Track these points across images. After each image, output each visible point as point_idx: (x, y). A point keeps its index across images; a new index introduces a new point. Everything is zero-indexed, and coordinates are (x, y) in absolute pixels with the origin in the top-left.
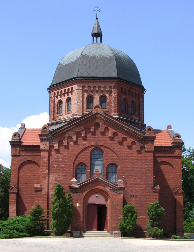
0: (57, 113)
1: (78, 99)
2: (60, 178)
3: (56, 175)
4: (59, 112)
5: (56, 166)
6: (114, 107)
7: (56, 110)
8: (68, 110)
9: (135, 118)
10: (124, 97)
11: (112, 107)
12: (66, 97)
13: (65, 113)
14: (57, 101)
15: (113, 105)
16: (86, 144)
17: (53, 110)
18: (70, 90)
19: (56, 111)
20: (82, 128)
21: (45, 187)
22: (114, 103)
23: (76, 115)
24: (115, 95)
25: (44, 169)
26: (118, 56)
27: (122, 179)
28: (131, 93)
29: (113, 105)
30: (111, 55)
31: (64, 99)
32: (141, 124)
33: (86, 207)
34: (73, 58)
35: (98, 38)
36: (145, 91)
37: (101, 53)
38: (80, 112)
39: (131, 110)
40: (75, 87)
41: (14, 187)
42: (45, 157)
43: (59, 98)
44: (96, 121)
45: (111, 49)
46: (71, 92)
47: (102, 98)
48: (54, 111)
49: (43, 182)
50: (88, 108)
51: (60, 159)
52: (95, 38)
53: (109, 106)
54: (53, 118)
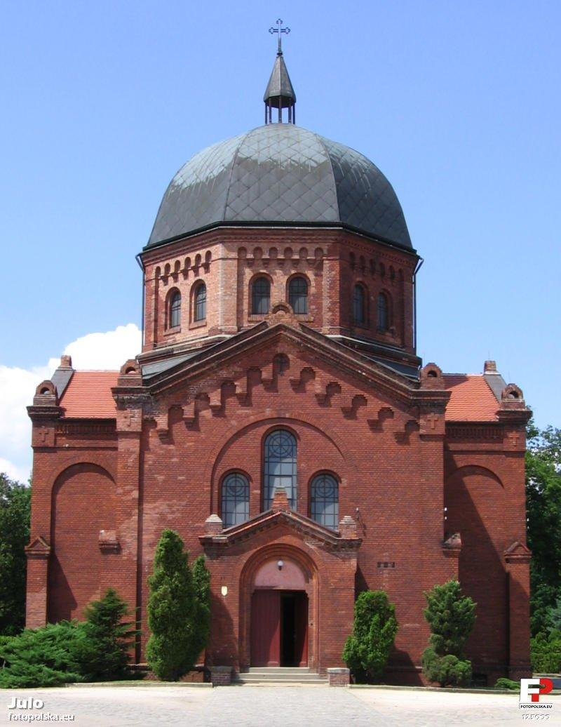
0: (166, 325)
1: (226, 287)
2: (173, 512)
3: (162, 506)
4: (171, 323)
5: (160, 478)
6: (330, 310)
7: (163, 316)
8: (197, 316)
9: (392, 340)
10: (358, 279)
11: (325, 309)
12: (192, 279)
13: (187, 325)
14: (164, 290)
15: (326, 303)
16: (247, 416)
17: (153, 319)
18: (203, 261)
19: (162, 321)
20: (238, 369)
21: (130, 540)
22: (330, 297)
23: (221, 331)
24: (334, 273)
25: (128, 488)
26: (342, 161)
27: (353, 517)
28: (378, 267)
29: (326, 303)
30: (322, 159)
31: (185, 286)
32: (407, 357)
33: (247, 598)
34: (211, 167)
35: (283, 109)
36: (420, 261)
37: (293, 152)
38: (231, 323)
39: (378, 317)
40: (218, 250)
41: (41, 541)
42: (129, 453)
43: (171, 283)
44: (279, 350)
45: (322, 142)
46: (206, 266)
47: (295, 284)
48: (156, 321)
49: (124, 526)
50: (254, 310)
51: (175, 460)
52: (275, 111)
53: (314, 307)
54: (152, 339)
